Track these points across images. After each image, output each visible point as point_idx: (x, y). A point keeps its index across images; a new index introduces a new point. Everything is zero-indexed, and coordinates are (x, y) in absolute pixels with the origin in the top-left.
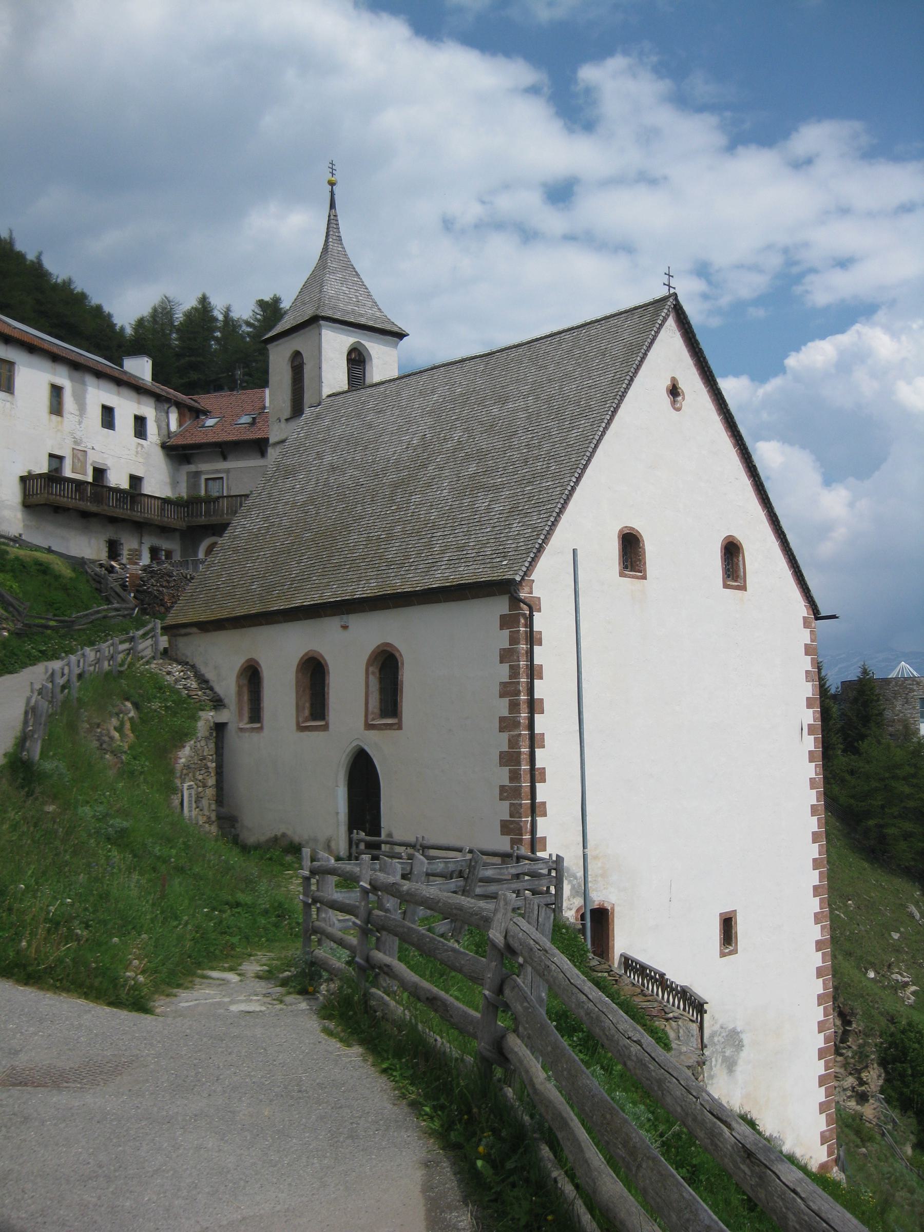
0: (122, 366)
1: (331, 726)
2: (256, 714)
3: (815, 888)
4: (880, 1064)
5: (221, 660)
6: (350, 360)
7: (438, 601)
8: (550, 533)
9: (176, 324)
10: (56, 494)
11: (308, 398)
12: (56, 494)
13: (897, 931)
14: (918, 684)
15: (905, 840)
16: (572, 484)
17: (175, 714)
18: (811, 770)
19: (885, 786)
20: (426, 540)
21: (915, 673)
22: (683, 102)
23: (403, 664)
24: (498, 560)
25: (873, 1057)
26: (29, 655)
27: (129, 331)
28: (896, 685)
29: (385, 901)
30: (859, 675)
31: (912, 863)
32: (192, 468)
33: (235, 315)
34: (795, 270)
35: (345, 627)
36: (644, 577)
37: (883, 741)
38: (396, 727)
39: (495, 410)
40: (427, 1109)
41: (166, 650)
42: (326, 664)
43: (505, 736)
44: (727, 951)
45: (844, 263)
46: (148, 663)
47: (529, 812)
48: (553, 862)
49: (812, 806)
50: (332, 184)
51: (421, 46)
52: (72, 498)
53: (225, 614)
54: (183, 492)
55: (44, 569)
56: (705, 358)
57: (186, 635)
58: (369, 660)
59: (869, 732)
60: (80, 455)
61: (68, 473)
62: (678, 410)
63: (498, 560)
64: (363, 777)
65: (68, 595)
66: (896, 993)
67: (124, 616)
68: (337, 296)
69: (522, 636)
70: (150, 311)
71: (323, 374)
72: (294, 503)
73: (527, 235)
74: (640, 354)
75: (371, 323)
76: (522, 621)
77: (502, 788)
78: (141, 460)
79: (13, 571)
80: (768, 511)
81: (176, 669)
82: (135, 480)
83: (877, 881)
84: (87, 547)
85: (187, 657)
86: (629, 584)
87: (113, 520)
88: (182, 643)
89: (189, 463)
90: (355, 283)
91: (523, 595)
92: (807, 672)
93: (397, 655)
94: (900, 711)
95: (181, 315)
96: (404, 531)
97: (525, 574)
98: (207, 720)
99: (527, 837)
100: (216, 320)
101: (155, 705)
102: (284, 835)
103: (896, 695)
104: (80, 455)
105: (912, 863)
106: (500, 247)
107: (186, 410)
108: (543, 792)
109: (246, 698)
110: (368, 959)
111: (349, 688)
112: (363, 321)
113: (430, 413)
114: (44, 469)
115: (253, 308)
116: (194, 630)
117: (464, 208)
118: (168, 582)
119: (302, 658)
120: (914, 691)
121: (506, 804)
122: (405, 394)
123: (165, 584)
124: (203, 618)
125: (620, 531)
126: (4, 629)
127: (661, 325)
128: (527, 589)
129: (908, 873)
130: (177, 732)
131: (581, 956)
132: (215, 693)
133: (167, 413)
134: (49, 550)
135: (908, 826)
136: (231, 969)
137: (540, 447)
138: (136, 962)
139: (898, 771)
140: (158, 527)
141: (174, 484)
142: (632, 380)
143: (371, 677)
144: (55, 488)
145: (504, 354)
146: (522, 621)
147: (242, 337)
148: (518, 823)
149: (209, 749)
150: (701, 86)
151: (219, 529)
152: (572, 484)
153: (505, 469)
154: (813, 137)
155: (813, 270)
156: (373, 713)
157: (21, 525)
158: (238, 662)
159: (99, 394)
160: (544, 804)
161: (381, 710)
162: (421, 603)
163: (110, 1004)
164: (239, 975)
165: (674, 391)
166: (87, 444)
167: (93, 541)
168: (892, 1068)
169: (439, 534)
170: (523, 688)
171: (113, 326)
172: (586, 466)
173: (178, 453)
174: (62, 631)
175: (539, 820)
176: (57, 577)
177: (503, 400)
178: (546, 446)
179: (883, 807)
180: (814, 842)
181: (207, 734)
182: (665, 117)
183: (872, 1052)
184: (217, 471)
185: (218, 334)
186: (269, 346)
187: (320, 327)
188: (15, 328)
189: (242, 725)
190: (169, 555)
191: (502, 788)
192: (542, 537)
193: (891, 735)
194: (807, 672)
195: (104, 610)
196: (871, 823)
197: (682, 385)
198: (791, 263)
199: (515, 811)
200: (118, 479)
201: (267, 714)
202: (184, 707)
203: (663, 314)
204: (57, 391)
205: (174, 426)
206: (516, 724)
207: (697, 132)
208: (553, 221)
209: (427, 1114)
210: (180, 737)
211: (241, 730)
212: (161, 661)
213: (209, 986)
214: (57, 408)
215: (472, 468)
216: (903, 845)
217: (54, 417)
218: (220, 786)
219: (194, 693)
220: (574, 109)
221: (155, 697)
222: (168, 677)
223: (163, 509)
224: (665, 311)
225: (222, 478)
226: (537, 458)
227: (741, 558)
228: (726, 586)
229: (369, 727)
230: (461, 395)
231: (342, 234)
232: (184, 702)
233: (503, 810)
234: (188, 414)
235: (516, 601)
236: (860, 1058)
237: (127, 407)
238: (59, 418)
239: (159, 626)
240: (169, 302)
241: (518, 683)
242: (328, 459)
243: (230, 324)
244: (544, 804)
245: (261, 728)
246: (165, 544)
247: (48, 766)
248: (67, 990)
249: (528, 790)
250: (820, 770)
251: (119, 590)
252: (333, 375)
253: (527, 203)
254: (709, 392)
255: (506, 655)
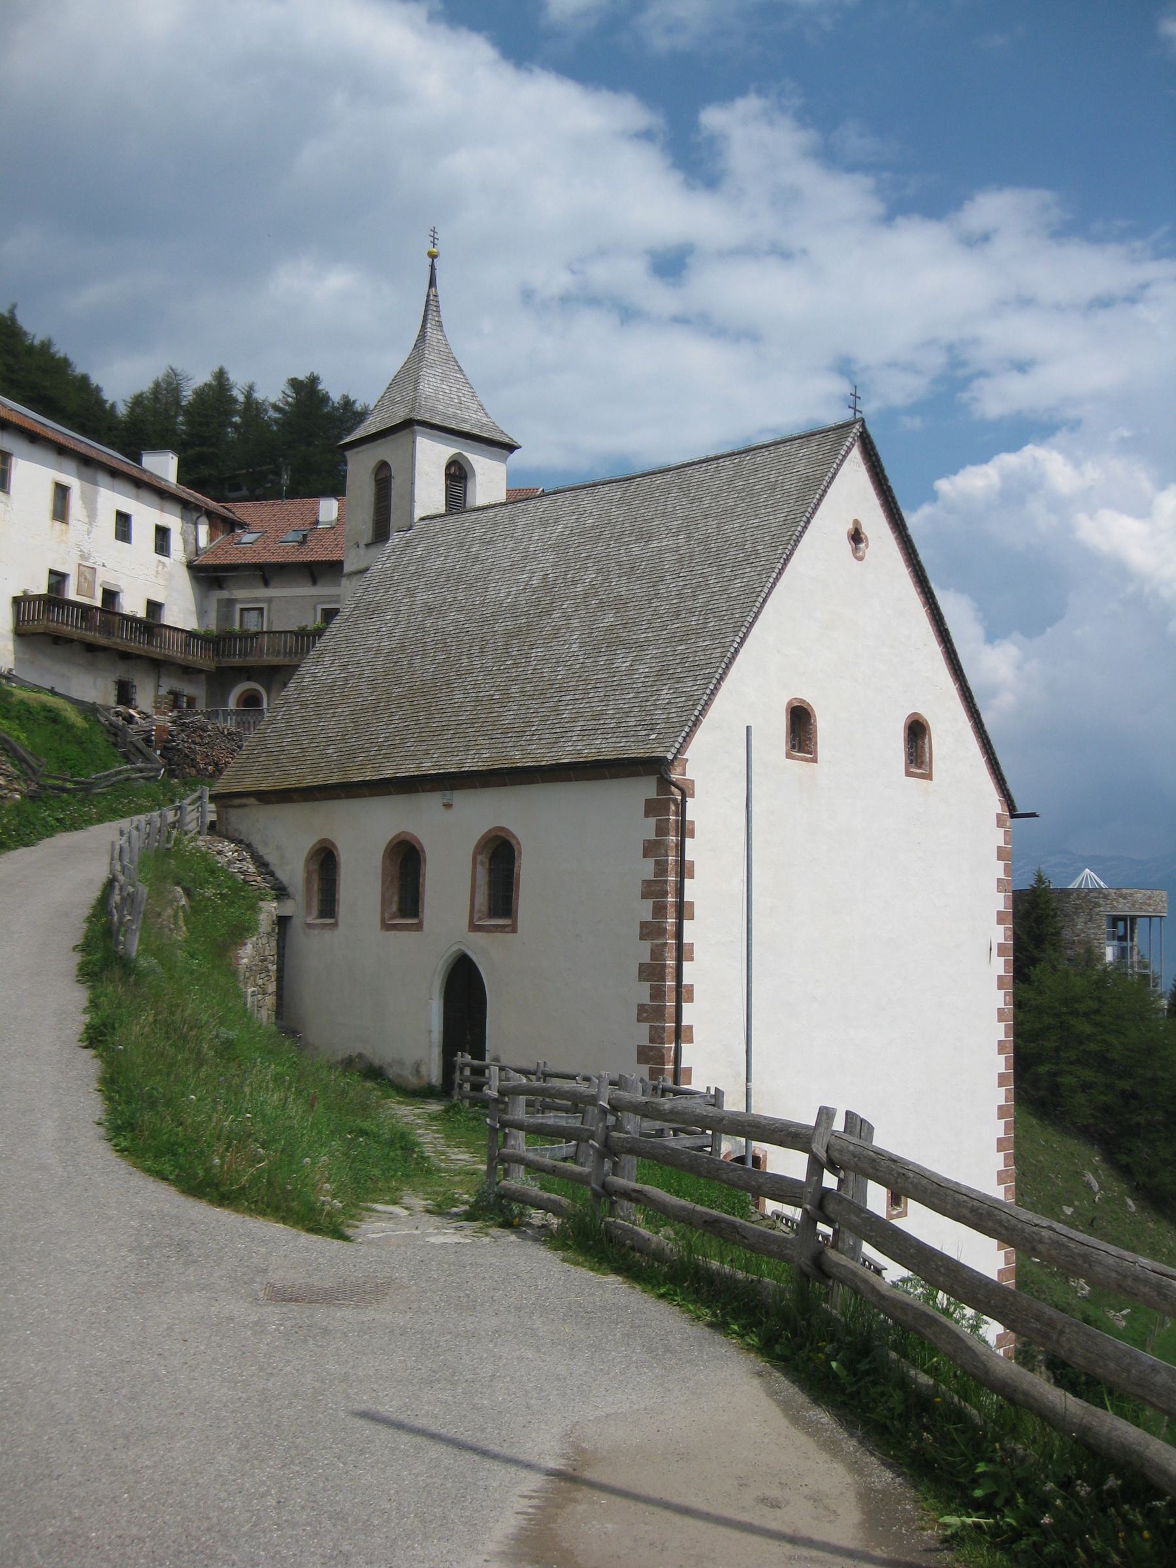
0: (138, 461)
1: (340, 924)
2: (328, 906)
3: (1000, 1141)
4: (1048, 1368)
5: (288, 839)
6: (449, 476)
7: (568, 779)
8: (707, 704)
9: (184, 403)
10: (58, 621)
11: (395, 519)
12: (58, 621)
13: (1070, 1205)
14: (1106, 897)
15: (1083, 1091)
16: (736, 645)
17: (231, 904)
18: (999, 999)
19: (1061, 1023)
20: (552, 704)
21: (1102, 884)
22: (830, 157)
23: (520, 853)
24: (644, 733)
25: (1041, 1357)
26: (45, 824)
27: (122, 410)
28: (1078, 898)
29: (625, 1123)
30: (1033, 882)
31: (1091, 1121)
32: (224, 594)
33: (259, 395)
34: (961, 373)
35: (448, 806)
36: (815, 760)
37: (1060, 967)
38: (510, 929)
39: (636, 548)
40: (736, 1327)
41: (212, 822)
42: (423, 851)
43: (647, 945)
44: (895, 1212)
45: (1022, 366)
46: (193, 839)
47: (673, 1037)
48: (712, 1096)
49: (1000, 1042)
50: (433, 256)
51: (507, 72)
52: (76, 626)
53: (293, 783)
54: (212, 625)
55: (54, 717)
56: (893, 498)
57: (239, 806)
58: (477, 847)
59: (1042, 955)
60: (88, 573)
61: (71, 594)
62: (860, 559)
63: (644, 733)
64: (464, 990)
65: (83, 750)
66: (1067, 1281)
67: (148, 779)
68: (437, 395)
69: (672, 826)
70: (151, 385)
71: (417, 491)
72: (379, 651)
73: (628, 314)
74: (819, 491)
75: (476, 431)
76: (673, 808)
77: (641, 1008)
78: (162, 582)
79: (18, 718)
80: (960, 685)
81: (228, 848)
82: (154, 607)
83: (1046, 1142)
84: (93, 687)
85: (240, 833)
86: (797, 767)
87: (125, 656)
88: (234, 815)
89: (221, 587)
90: (457, 380)
91: (674, 776)
92: (999, 880)
93: (514, 842)
94: (1081, 930)
95: (190, 393)
96: (523, 692)
97: (678, 751)
98: (270, 913)
99: (670, 1067)
100: (235, 401)
101: (209, 892)
102: (360, 1056)
103: (1077, 910)
104: (87, 572)
105: (1091, 1121)
106: (592, 327)
107: (219, 521)
108: (690, 1014)
109: (316, 887)
110: (604, 1186)
111: (450, 882)
112: (466, 427)
113: (554, 547)
114: (43, 589)
115: (283, 388)
116: (252, 801)
117: (570, 285)
118: (202, 737)
119: (391, 841)
120: (1100, 906)
121: (645, 1026)
122: (521, 522)
123: (198, 740)
124: (264, 787)
125: (789, 703)
126: (16, 790)
127: (845, 457)
128: (679, 770)
129: (1087, 1134)
130: (236, 926)
131: (743, 1208)
132: (277, 879)
133: (196, 524)
134: (52, 692)
135: (1088, 1074)
136: (395, 1203)
137: (694, 597)
138: (327, 1186)
139: (1077, 1005)
140: (180, 666)
141: (201, 613)
142: (808, 522)
143: (479, 868)
144: (56, 614)
145: (647, 480)
146: (673, 808)
147: (269, 425)
148: (660, 1050)
149: (270, 949)
150: (854, 139)
151: (276, 675)
152: (736, 645)
153: (650, 622)
154: (991, 208)
155: (984, 374)
156: (480, 912)
157: (12, 657)
158: (309, 842)
159: (112, 499)
160: (690, 1027)
161: (490, 908)
162: (546, 780)
163: (310, 1230)
164: (406, 1208)
165: (856, 537)
166: (96, 560)
167: (100, 682)
168: (1061, 1374)
169: (568, 698)
170: (670, 888)
171: (101, 403)
172: (752, 624)
173: (207, 576)
174: (80, 795)
175: (685, 1047)
176: (70, 727)
177: (646, 537)
178: (703, 597)
179: (1057, 1050)
180: (1000, 1085)
181: (269, 929)
182: (806, 175)
183: (1039, 1352)
184: (257, 600)
185: (237, 419)
186: (348, 454)
187: (414, 434)
188: (11, 410)
189: (310, 920)
190: (191, 702)
191: (641, 1008)
192: (699, 708)
193: (1069, 960)
194: (999, 880)
195: (126, 770)
196: (1042, 1069)
197: (866, 530)
198: (956, 363)
199: (656, 1035)
200: (132, 605)
201: (342, 909)
202: (240, 895)
203: (848, 444)
204: (62, 492)
205: (203, 541)
206: (662, 932)
207: (846, 196)
208: (660, 299)
209: (735, 1332)
210: (240, 932)
211: (309, 926)
212: (208, 838)
213: (379, 1219)
214: (61, 512)
215: (609, 619)
216: (1081, 1098)
217: (57, 524)
218: (280, 994)
219: (252, 878)
220: (694, 160)
221: (208, 882)
222: (218, 858)
223: (187, 645)
224: (850, 439)
225: (261, 609)
226: (691, 611)
227: (926, 741)
228: (909, 774)
229: (474, 927)
230: (593, 527)
231: (443, 319)
232: (241, 889)
233: (642, 1034)
234: (220, 525)
235: (665, 784)
236: (1024, 1358)
237: (147, 516)
238: (63, 526)
239: (207, 794)
240: (176, 375)
241: (666, 882)
242: (422, 597)
243: (252, 407)
244: (690, 1027)
245: (336, 925)
246: (188, 689)
247: (143, 963)
248: (263, 1213)
249: (673, 1010)
250: (1010, 999)
251: (141, 745)
252: (429, 494)
253: (628, 275)
254: (896, 538)
255: (652, 848)
